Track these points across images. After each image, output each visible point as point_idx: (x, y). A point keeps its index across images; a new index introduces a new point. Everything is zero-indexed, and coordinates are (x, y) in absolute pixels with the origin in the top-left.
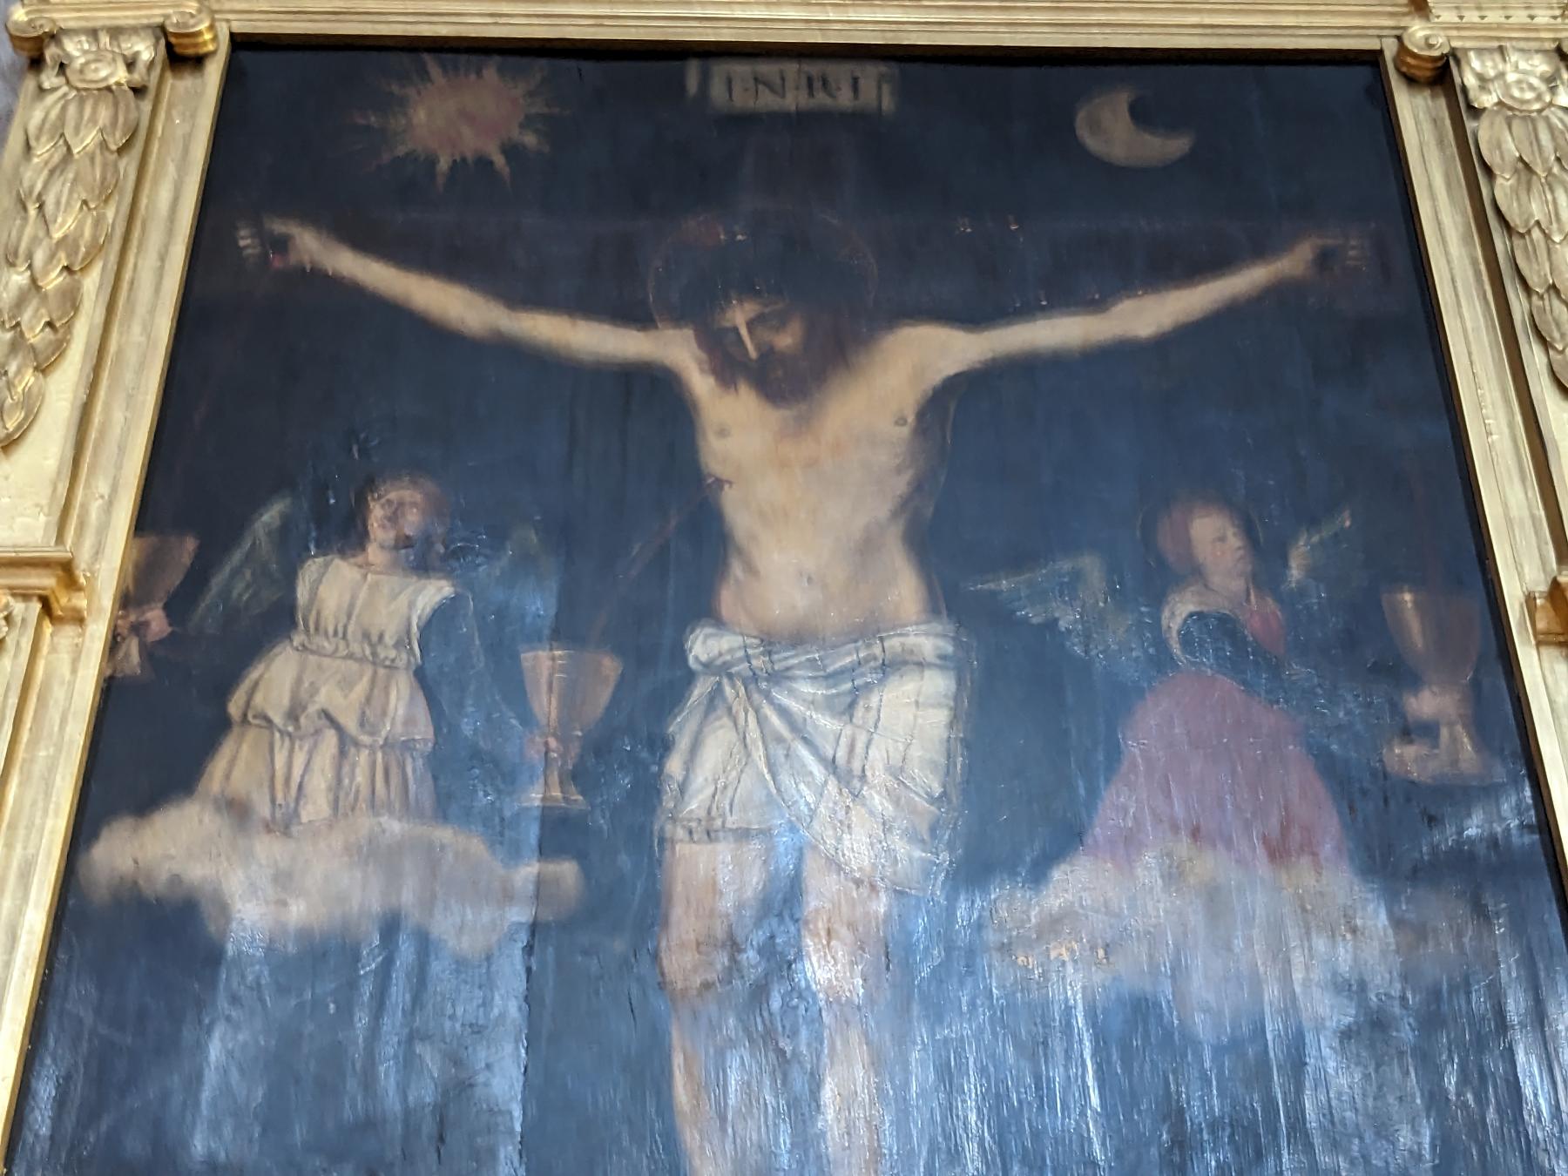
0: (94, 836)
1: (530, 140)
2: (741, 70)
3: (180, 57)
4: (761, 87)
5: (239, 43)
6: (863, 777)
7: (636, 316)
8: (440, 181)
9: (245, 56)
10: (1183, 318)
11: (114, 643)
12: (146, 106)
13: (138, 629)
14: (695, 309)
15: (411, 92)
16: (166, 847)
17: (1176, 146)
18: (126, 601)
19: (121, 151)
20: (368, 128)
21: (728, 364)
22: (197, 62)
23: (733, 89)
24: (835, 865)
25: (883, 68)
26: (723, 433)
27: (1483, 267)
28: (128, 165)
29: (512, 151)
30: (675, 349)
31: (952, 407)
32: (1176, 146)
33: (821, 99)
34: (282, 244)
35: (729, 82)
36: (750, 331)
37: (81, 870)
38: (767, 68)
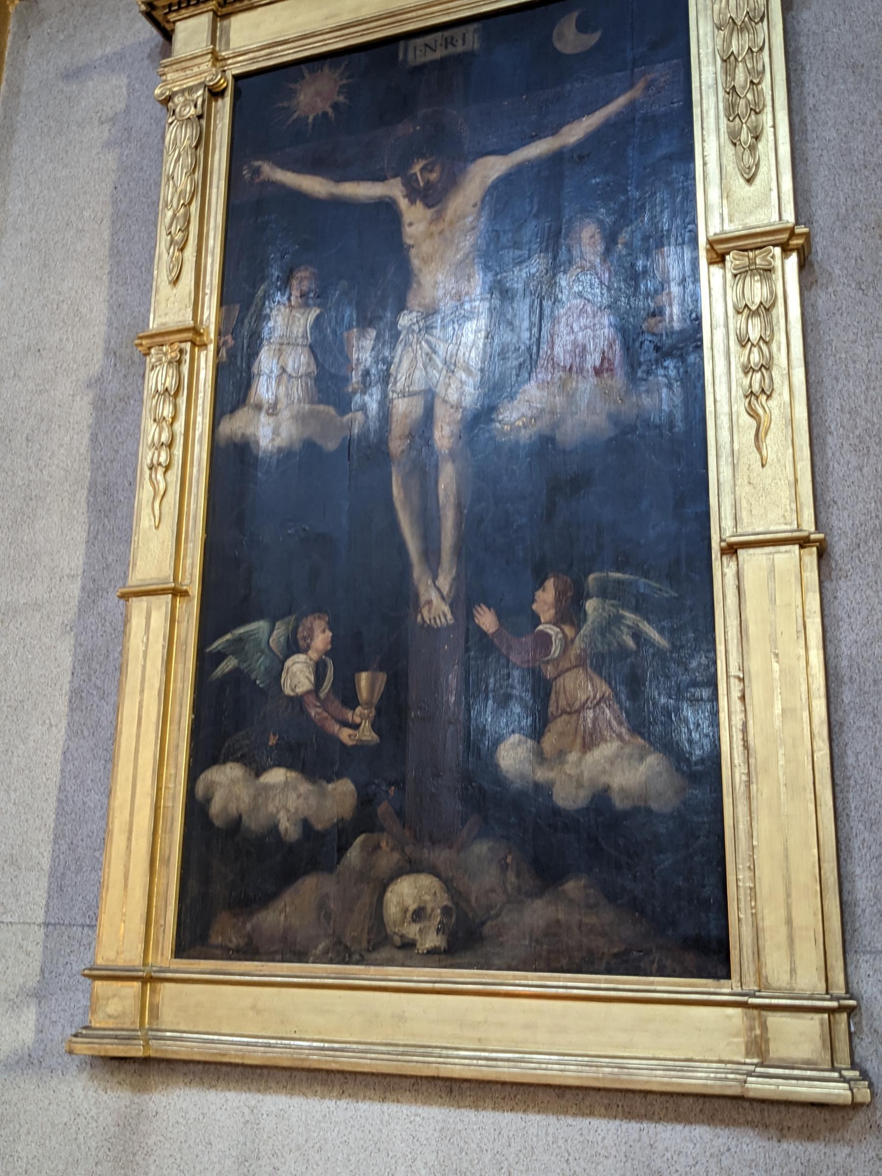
0: (219, 423)
1: (341, 99)
2: (419, 41)
3: (215, 94)
4: (428, 49)
5: (237, 78)
6: (455, 365)
7: (380, 178)
8: (310, 126)
9: (240, 83)
10: (590, 129)
11: (218, 351)
12: (204, 122)
13: (225, 343)
14: (401, 170)
15: (297, 86)
16: (236, 425)
17: (593, 39)
18: (219, 333)
19: (196, 147)
20: (283, 108)
21: (414, 193)
22: (221, 94)
23: (417, 54)
24: (445, 401)
25: (475, 26)
26: (411, 224)
27: (155, 267)
28: (201, 152)
29: (335, 106)
30: (393, 189)
31: (501, 195)
32: (593, 39)
33: (451, 50)
34: (257, 171)
35: (415, 48)
36: (421, 174)
37: (216, 438)
38: (429, 39)
